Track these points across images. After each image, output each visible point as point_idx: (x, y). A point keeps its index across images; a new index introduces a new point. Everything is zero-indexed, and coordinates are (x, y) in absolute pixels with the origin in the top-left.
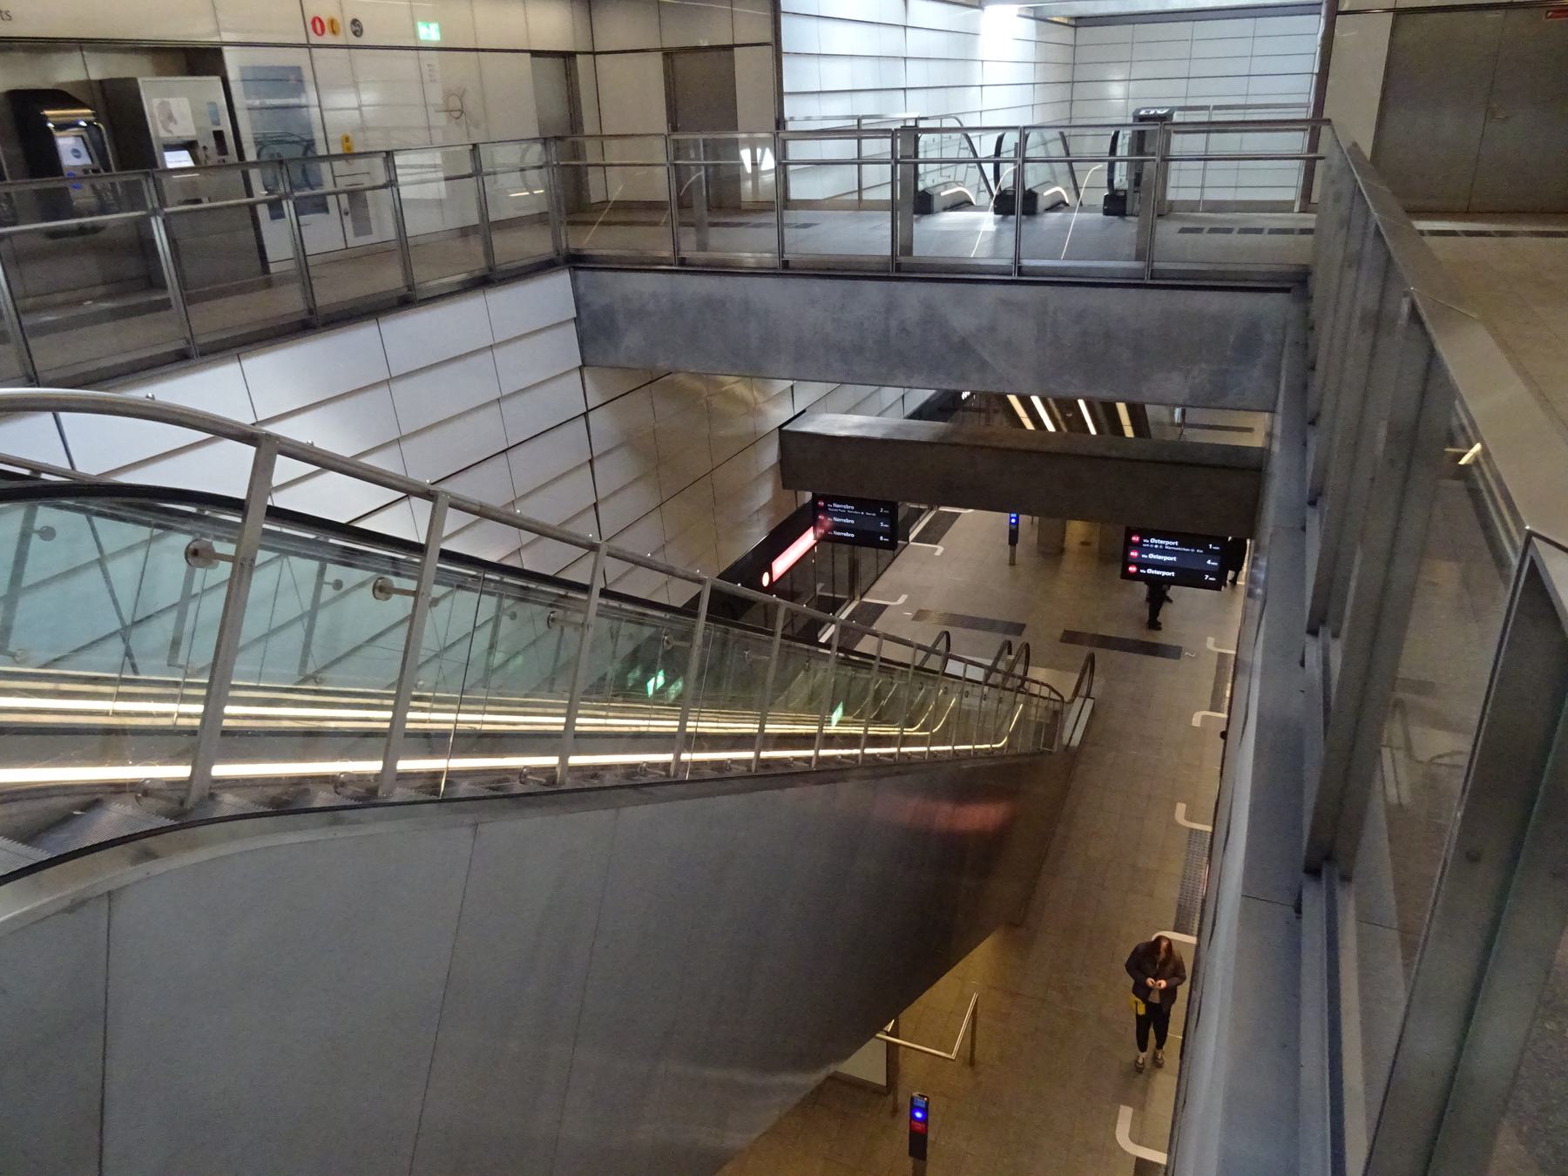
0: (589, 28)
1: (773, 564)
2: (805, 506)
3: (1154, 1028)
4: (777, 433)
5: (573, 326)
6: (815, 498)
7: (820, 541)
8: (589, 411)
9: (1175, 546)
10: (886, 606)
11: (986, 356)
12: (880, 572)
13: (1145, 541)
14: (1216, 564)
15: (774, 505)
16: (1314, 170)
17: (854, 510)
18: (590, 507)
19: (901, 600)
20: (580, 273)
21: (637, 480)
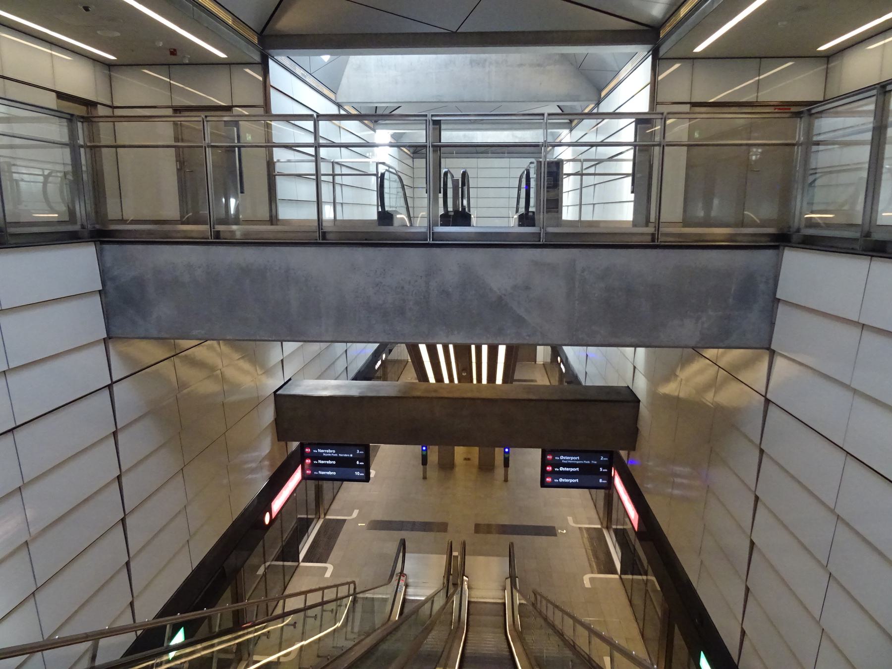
0: (109, 89)
1: (272, 503)
2: (293, 453)
4: (272, 398)
5: (97, 298)
6: (302, 447)
7: (305, 477)
8: (113, 383)
9: (577, 460)
10: (345, 521)
11: (521, 312)
12: (335, 494)
15: (270, 456)
16: (567, 233)
17: (334, 453)
18: (115, 478)
19: (355, 513)
20: (107, 247)
21: (161, 447)
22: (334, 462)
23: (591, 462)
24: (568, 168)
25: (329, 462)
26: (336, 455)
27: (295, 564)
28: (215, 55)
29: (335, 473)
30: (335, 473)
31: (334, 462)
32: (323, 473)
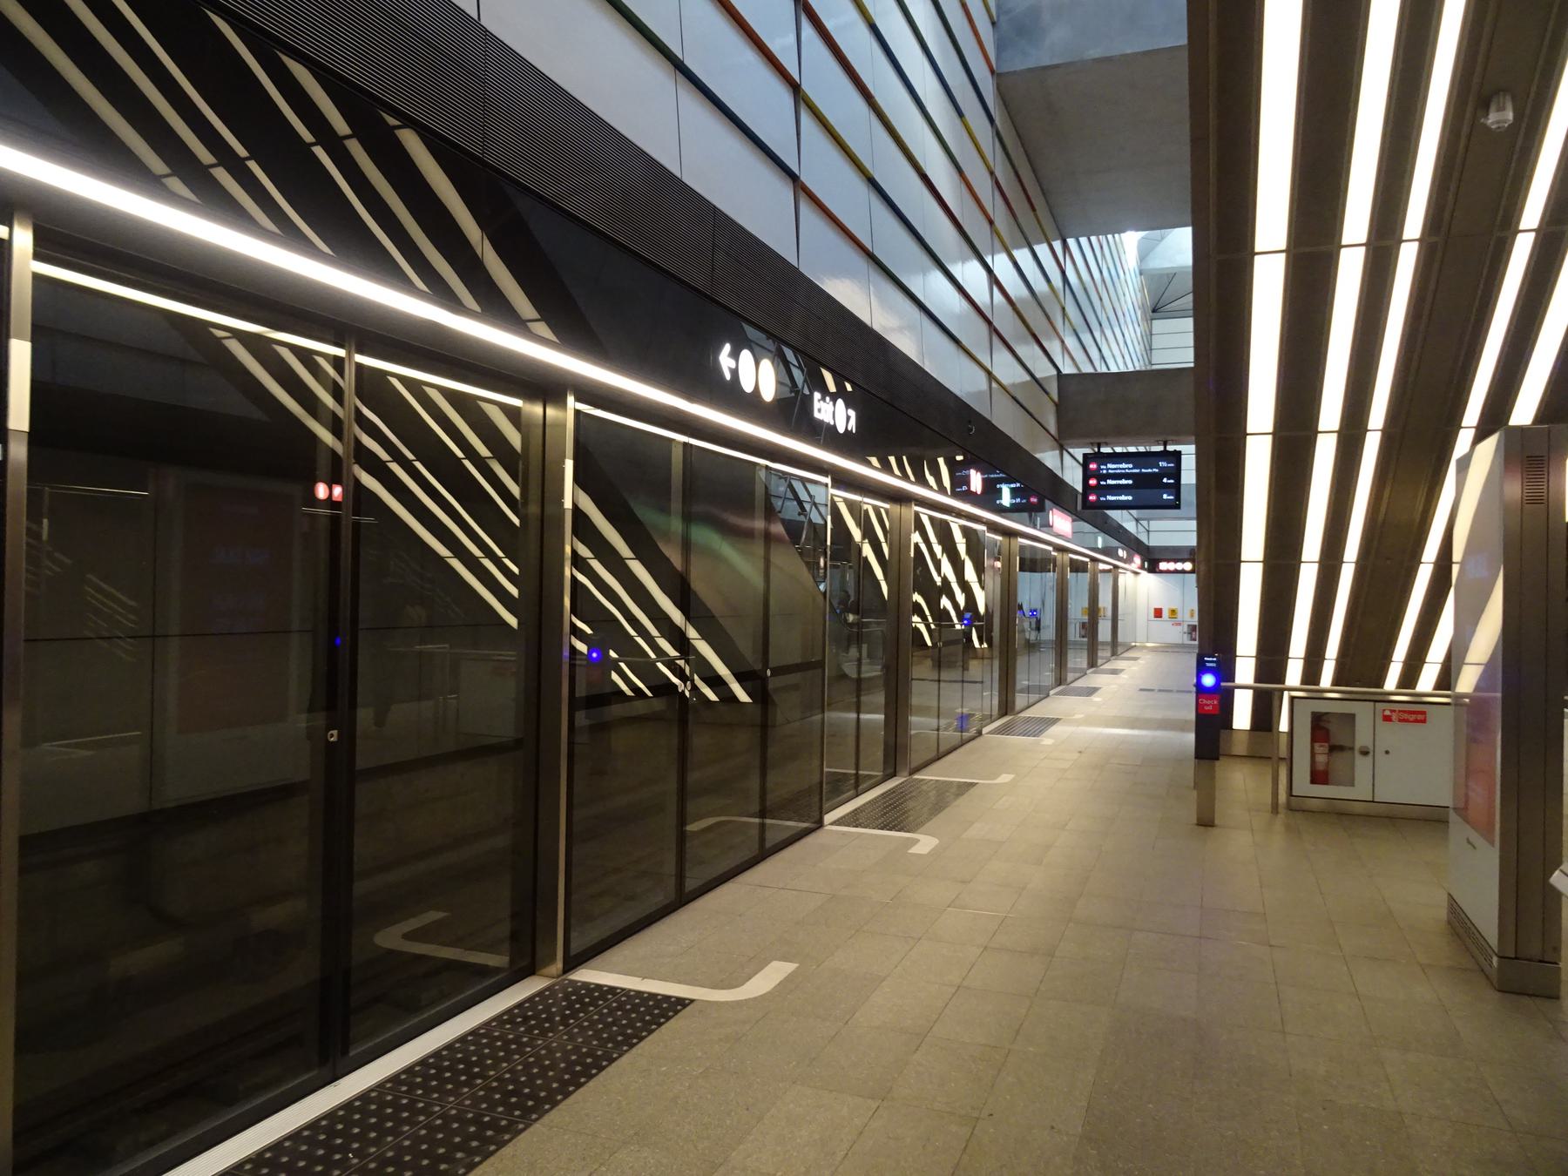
3: (883, 595)
13: (1102, 467)
14: (1172, 465)
22: (1130, 482)
24: (551, 412)
25: (1123, 482)
28: (1320, 679)
30: (1130, 498)
31: (1130, 482)
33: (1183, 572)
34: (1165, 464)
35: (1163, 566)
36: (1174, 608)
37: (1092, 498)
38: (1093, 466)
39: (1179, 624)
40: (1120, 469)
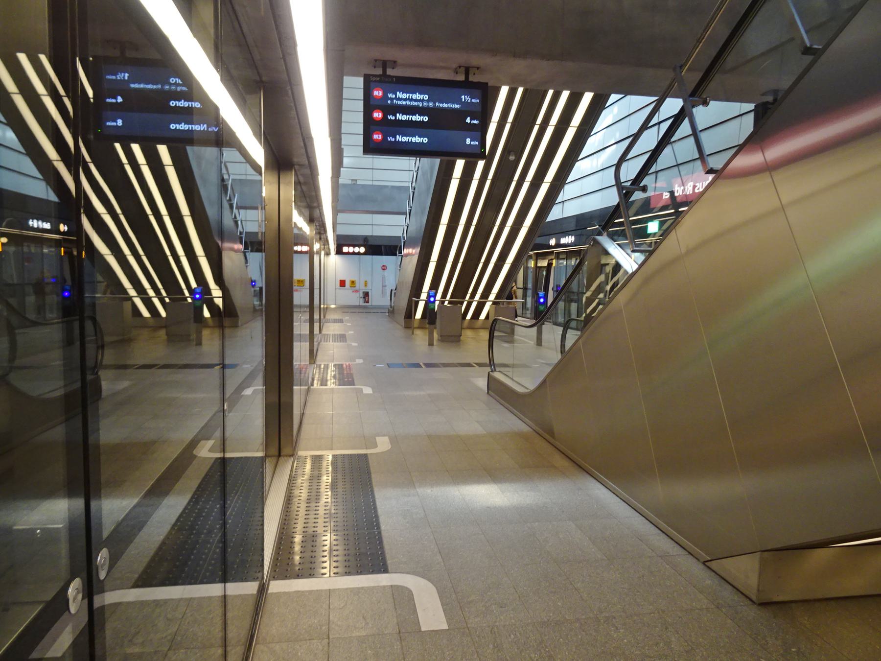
22: (426, 119)
23: (435, 103)
25: (417, 118)
26: (431, 104)
27: (250, 588)
29: (425, 140)
30: (425, 140)
31: (426, 119)
32: (404, 139)
33: (359, 253)
34: (468, 99)
35: (345, 249)
36: (353, 279)
37: (377, 137)
38: (378, 93)
39: (357, 291)
40: (411, 100)
